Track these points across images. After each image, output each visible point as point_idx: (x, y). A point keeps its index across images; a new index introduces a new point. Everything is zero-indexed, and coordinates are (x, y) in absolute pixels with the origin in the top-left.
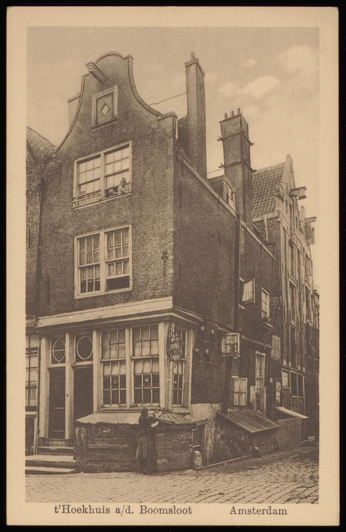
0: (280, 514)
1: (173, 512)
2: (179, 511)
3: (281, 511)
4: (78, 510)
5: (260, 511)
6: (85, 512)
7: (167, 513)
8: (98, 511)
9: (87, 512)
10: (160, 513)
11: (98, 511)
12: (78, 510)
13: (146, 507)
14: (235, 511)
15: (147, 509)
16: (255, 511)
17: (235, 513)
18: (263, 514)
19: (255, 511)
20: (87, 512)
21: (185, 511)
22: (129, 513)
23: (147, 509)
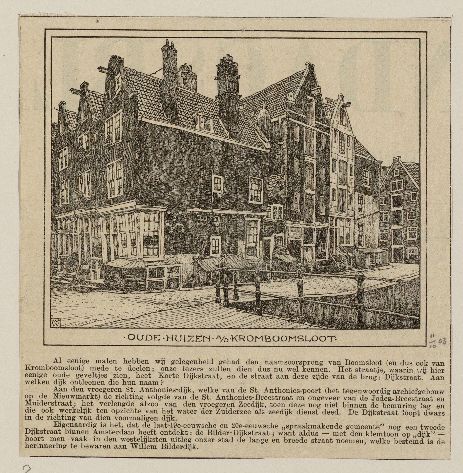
0: (123, 448)
1: (68, 369)
2: (72, 368)
3: (130, 432)
4: (212, 405)
5: (193, 411)
6: (28, 369)
7: (311, 414)
8: (264, 370)
9: (246, 435)
10: (313, 400)
11: (264, 370)
12: (212, 405)
13: (350, 361)
14: (143, 390)
15: (350, 362)
16: (189, 412)
17: (143, 391)
18: (224, 406)
19: (189, 412)
20: (246, 435)
21: (76, 368)
22: (338, 414)
23: (350, 362)
